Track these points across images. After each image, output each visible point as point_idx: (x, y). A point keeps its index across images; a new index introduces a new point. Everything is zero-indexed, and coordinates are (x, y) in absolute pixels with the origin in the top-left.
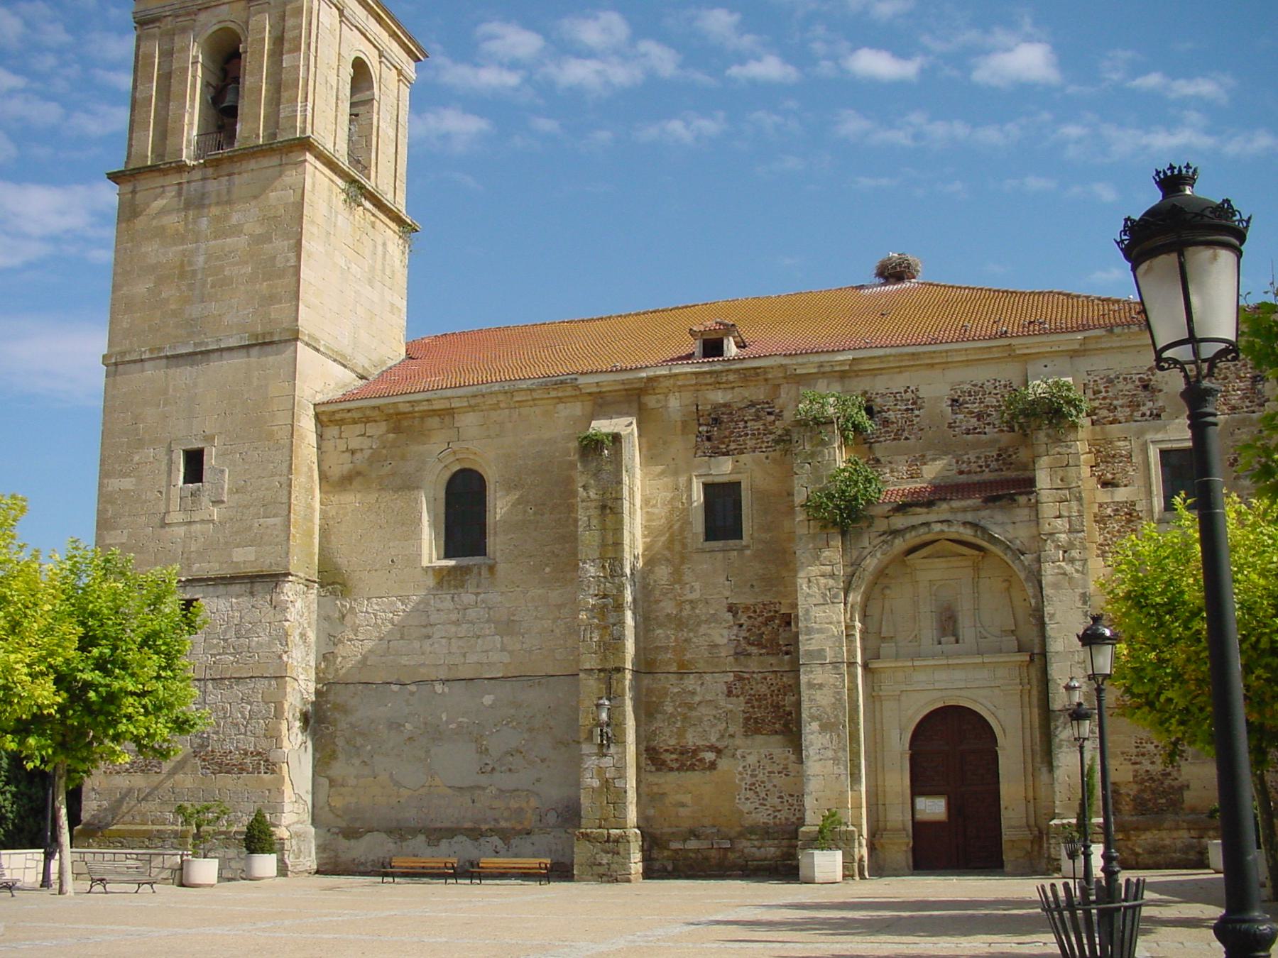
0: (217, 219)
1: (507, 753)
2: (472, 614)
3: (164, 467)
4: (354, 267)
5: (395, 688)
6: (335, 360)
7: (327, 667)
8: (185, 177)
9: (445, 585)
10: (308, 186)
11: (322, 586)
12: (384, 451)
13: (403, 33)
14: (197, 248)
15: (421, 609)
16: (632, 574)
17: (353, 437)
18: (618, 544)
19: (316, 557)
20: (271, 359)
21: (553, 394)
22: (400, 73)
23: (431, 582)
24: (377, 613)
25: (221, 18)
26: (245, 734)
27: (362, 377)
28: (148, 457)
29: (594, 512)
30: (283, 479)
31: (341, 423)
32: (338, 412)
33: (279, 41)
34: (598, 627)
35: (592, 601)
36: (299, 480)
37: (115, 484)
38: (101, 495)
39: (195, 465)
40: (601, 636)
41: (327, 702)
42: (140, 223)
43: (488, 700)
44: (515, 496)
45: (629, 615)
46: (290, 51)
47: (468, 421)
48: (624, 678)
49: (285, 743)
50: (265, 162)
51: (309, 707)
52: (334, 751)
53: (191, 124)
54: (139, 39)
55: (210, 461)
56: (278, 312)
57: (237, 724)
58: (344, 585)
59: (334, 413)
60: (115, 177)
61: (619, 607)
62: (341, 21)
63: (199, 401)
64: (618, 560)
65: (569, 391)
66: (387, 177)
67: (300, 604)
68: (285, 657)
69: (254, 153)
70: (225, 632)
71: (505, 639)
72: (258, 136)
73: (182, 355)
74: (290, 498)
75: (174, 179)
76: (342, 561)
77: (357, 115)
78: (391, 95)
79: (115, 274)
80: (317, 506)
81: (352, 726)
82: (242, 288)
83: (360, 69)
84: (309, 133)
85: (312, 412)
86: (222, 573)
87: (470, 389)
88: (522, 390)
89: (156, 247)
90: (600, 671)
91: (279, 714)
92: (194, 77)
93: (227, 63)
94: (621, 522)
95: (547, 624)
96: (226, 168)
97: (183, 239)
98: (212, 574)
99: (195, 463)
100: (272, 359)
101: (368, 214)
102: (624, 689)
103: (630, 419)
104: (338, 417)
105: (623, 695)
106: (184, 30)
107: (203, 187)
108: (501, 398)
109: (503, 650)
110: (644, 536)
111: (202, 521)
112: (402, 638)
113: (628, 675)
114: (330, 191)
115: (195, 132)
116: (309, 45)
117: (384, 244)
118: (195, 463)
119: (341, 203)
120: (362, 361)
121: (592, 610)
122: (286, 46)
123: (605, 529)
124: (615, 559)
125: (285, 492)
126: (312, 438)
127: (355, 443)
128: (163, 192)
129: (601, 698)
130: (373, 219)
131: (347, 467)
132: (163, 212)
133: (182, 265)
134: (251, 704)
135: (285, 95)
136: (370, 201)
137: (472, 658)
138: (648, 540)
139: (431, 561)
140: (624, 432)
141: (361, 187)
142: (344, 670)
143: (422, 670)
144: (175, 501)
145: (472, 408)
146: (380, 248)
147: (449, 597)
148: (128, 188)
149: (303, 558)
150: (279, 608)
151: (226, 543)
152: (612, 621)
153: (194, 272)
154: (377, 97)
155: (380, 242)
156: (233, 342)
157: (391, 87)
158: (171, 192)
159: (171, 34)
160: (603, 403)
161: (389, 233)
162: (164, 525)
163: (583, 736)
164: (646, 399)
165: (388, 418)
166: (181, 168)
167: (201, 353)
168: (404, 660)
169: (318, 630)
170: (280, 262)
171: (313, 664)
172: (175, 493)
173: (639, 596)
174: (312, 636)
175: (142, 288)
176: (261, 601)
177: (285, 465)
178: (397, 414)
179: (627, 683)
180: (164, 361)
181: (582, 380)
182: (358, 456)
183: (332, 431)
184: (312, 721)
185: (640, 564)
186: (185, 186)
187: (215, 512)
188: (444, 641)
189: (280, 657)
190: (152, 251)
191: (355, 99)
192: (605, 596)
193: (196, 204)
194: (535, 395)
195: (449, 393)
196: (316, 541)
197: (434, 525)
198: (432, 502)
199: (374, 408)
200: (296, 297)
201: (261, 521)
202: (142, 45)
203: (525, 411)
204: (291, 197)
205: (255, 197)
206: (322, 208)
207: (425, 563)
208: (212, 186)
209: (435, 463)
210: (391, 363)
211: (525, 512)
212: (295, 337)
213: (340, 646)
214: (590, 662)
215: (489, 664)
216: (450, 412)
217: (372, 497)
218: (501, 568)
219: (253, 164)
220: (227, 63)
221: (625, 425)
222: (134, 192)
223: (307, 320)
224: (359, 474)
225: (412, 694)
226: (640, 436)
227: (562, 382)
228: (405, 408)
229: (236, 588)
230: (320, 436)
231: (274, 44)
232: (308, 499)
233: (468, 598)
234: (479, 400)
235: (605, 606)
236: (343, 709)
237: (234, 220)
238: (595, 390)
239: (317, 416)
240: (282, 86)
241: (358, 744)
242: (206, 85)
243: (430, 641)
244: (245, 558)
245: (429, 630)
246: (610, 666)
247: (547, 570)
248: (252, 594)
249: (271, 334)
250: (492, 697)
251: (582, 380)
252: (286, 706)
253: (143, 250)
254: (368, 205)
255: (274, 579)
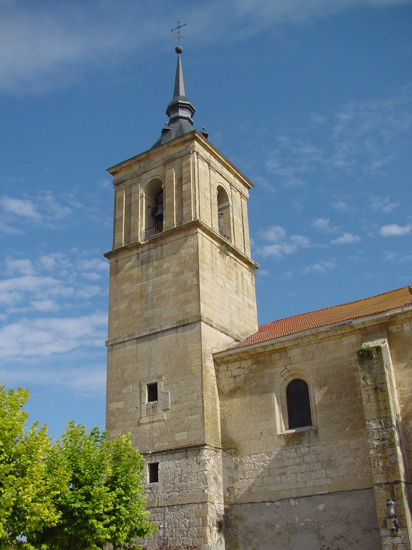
0: (157, 267)
1: (335, 538)
2: (307, 458)
3: (138, 394)
4: (228, 286)
5: (268, 504)
6: (222, 332)
7: (230, 495)
8: (140, 250)
9: (291, 443)
10: (200, 245)
11: (224, 451)
12: (251, 375)
13: (241, 175)
14: (148, 283)
15: (279, 458)
16: (397, 425)
17: (234, 369)
18: (387, 409)
19: (220, 435)
20: (188, 332)
21: (339, 332)
22: (241, 194)
23: (283, 442)
24: (255, 463)
25: (153, 175)
26: (187, 536)
27: (237, 341)
28: (129, 390)
29: (371, 392)
30: (199, 394)
31: (227, 362)
32: (225, 357)
33: (180, 180)
34: (381, 458)
35: (376, 443)
36: (207, 394)
37: (115, 405)
38: (107, 412)
39: (153, 391)
40: (384, 464)
41: (231, 515)
42: (120, 275)
43: (321, 507)
44: (325, 389)
45: (398, 449)
46: (186, 183)
47: (295, 353)
48: (401, 487)
49: (209, 540)
50: (178, 236)
51: (222, 518)
52: (237, 544)
53: (142, 225)
54: (116, 192)
55: (161, 388)
56: (190, 308)
57: (182, 531)
58: (236, 449)
59: (223, 357)
60: (108, 255)
61: (392, 445)
62: (209, 169)
63: (153, 359)
64: (388, 418)
65: (348, 330)
66: (240, 239)
67: (212, 461)
68: (206, 491)
69: (172, 233)
70: (174, 479)
71: (328, 471)
72: (174, 225)
73: (144, 337)
74: (203, 404)
75: (135, 252)
76: (234, 436)
77: (222, 214)
78: (238, 205)
79: (110, 301)
80: (218, 408)
81: (246, 528)
82: (171, 299)
83: (221, 191)
84: (198, 218)
85: (211, 358)
86: (170, 447)
87: (294, 335)
88: (322, 332)
89: (128, 285)
90: (386, 484)
91: (204, 524)
92: (142, 204)
93: (157, 196)
94: (387, 396)
95: (351, 460)
96: (160, 242)
97: (140, 279)
98: (165, 448)
99: (153, 391)
100: (189, 332)
101: (232, 260)
102: (402, 494)
103: (383, 340)
104: (225, 359)
105: (401, 498)
106: (136, 183)
107: (149, 253)
108: (311, 338)
109: (327, 477)
110: (400, 404)
111: (159, 421)
112: (270, 475)
113: (403, 485)
114: (212, 247)
115: (144, 229)
116: (195, 179)
117: (242, 275)
118: (153, 391)
119: (218, 254)
120: (236, 332)
121: (377, 449)
122: (184, 181)
123: (378, 401)
124: (386, 417)
125: (201, 401)
126: (213, 372)
127: (235, 373)
128: (130, 259)
129: (389, 500)
130: (235, 262)
131: (232, 386)
132: (131, 268)
133: (141, 291)
134: (189, 518)
135: (185, 204)
136: (232, 253)
137: (310, 484)
138: (403, 406)
139: (282, 431)
140: (382, 346)
141: (227, 246)
142: (239, 496)
143: (282, 493)
144: (144, 411)
145: (296, 346)
146: (240, 276)
147: (294, 450)
148: (114, 260)
149: (212, 436)
150: (201, 464)
151: (172, 431)
152: (389, 453)
153: (148, 295)
154: (231, 204)
155: (239, 273)
156: (169, 327)
157: (238, 200)
158: (134, 258)
159: (130, 187)
160: (367, 333)
161: (244, 269)
162: (139, 424)
163: (381, 524)
164: (390, 328)
165: (252, 357)
166: (138, 246)
167: (153, 334)
168: (272, 488)
169: (224, 475)
170: (189, 283)
171: (222, 494)
172: (144, 407)
173: (402, 438)
174: (220, 478)
175: (122, 306)
176: (192, 461)
177: (199, 387)
178: (256, 354)
179: (403, 490)
180: (135, 341)
181: (354, 322)
182: (238, 379)
183: (223, 367)
184: (223, 527)
185: (400, 419)
186: (141, 255)
187: (165, 415)
188: (293, 475)
189: (204, 491)
190: (127, 288)
191: (220, 207)
192: (383, 440)
193: (146, 261)
194: (330, 334)
195: (283, 339)
196: (219, 427)
197: (282, 410)
198: (279, 399)
199: (244, 352)
200: (198, 299)
201: (189, 417)
202: (117, 194)
203: (324, 343)
204: (192, 251)
205: (174, 254)
206: (208, 256)
207: (279, 433)
208: (153, 252)
209: (279, 378)
210: (251, 334)
211: (331, 398)
212: (199, 320)
213: (236, 483)
214: (380, 479)
215: (320, 486)
216: (284, 350)
217: (248, 398)
218: (321, 431)
219: (172, 238)
220: (157, 196)
221: (383, 343)
222: (117, 261)
223: (205, 310)
224: (239, 388)
225: (278, 507)
226: (390, 348)
227: (343, 325)
228: (260, 350)
229: (178, 455)
230: (217, 371)
231: (178, 181)
232: (214, 404)
233: (304, 450)
234: (299, 341)
235: (384, 445)
236: (241, 519)
237: (165, 266)
238: (362, 326)
239: (214, 360)
240: (183, 200)
241: (250, 538)
242: (148, 207)
243: (285, 476)
244: (182, 438)
245: (284, 470)
246: (392, 480)
247: (347, 429)
248: (187, 457)
249: (187, 320)
250: (323, 505)
251: (354, 322)
252: (208, 519)
253: (122, 288)
254: (232, 255)
255: (197, 448)
